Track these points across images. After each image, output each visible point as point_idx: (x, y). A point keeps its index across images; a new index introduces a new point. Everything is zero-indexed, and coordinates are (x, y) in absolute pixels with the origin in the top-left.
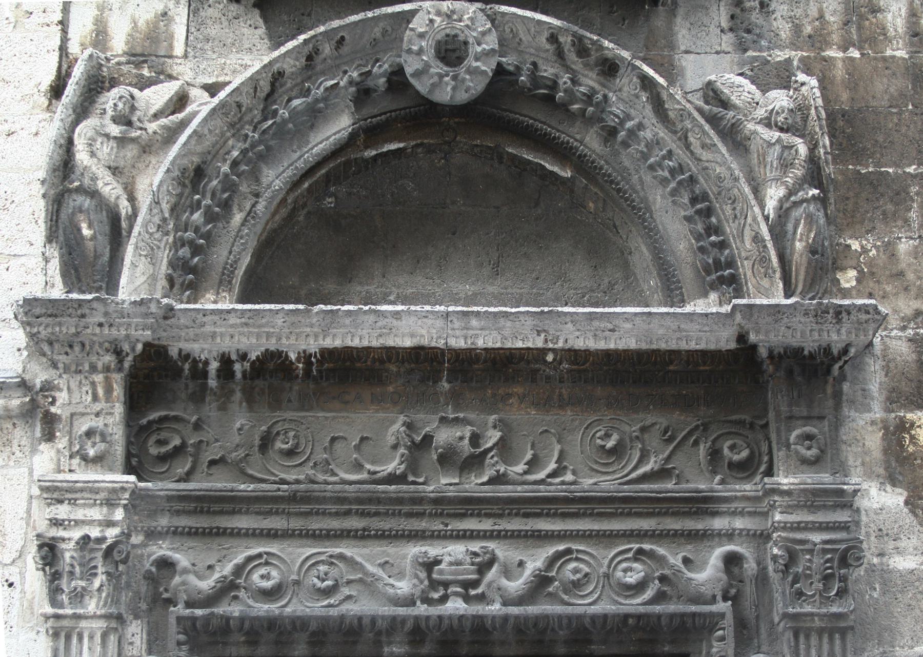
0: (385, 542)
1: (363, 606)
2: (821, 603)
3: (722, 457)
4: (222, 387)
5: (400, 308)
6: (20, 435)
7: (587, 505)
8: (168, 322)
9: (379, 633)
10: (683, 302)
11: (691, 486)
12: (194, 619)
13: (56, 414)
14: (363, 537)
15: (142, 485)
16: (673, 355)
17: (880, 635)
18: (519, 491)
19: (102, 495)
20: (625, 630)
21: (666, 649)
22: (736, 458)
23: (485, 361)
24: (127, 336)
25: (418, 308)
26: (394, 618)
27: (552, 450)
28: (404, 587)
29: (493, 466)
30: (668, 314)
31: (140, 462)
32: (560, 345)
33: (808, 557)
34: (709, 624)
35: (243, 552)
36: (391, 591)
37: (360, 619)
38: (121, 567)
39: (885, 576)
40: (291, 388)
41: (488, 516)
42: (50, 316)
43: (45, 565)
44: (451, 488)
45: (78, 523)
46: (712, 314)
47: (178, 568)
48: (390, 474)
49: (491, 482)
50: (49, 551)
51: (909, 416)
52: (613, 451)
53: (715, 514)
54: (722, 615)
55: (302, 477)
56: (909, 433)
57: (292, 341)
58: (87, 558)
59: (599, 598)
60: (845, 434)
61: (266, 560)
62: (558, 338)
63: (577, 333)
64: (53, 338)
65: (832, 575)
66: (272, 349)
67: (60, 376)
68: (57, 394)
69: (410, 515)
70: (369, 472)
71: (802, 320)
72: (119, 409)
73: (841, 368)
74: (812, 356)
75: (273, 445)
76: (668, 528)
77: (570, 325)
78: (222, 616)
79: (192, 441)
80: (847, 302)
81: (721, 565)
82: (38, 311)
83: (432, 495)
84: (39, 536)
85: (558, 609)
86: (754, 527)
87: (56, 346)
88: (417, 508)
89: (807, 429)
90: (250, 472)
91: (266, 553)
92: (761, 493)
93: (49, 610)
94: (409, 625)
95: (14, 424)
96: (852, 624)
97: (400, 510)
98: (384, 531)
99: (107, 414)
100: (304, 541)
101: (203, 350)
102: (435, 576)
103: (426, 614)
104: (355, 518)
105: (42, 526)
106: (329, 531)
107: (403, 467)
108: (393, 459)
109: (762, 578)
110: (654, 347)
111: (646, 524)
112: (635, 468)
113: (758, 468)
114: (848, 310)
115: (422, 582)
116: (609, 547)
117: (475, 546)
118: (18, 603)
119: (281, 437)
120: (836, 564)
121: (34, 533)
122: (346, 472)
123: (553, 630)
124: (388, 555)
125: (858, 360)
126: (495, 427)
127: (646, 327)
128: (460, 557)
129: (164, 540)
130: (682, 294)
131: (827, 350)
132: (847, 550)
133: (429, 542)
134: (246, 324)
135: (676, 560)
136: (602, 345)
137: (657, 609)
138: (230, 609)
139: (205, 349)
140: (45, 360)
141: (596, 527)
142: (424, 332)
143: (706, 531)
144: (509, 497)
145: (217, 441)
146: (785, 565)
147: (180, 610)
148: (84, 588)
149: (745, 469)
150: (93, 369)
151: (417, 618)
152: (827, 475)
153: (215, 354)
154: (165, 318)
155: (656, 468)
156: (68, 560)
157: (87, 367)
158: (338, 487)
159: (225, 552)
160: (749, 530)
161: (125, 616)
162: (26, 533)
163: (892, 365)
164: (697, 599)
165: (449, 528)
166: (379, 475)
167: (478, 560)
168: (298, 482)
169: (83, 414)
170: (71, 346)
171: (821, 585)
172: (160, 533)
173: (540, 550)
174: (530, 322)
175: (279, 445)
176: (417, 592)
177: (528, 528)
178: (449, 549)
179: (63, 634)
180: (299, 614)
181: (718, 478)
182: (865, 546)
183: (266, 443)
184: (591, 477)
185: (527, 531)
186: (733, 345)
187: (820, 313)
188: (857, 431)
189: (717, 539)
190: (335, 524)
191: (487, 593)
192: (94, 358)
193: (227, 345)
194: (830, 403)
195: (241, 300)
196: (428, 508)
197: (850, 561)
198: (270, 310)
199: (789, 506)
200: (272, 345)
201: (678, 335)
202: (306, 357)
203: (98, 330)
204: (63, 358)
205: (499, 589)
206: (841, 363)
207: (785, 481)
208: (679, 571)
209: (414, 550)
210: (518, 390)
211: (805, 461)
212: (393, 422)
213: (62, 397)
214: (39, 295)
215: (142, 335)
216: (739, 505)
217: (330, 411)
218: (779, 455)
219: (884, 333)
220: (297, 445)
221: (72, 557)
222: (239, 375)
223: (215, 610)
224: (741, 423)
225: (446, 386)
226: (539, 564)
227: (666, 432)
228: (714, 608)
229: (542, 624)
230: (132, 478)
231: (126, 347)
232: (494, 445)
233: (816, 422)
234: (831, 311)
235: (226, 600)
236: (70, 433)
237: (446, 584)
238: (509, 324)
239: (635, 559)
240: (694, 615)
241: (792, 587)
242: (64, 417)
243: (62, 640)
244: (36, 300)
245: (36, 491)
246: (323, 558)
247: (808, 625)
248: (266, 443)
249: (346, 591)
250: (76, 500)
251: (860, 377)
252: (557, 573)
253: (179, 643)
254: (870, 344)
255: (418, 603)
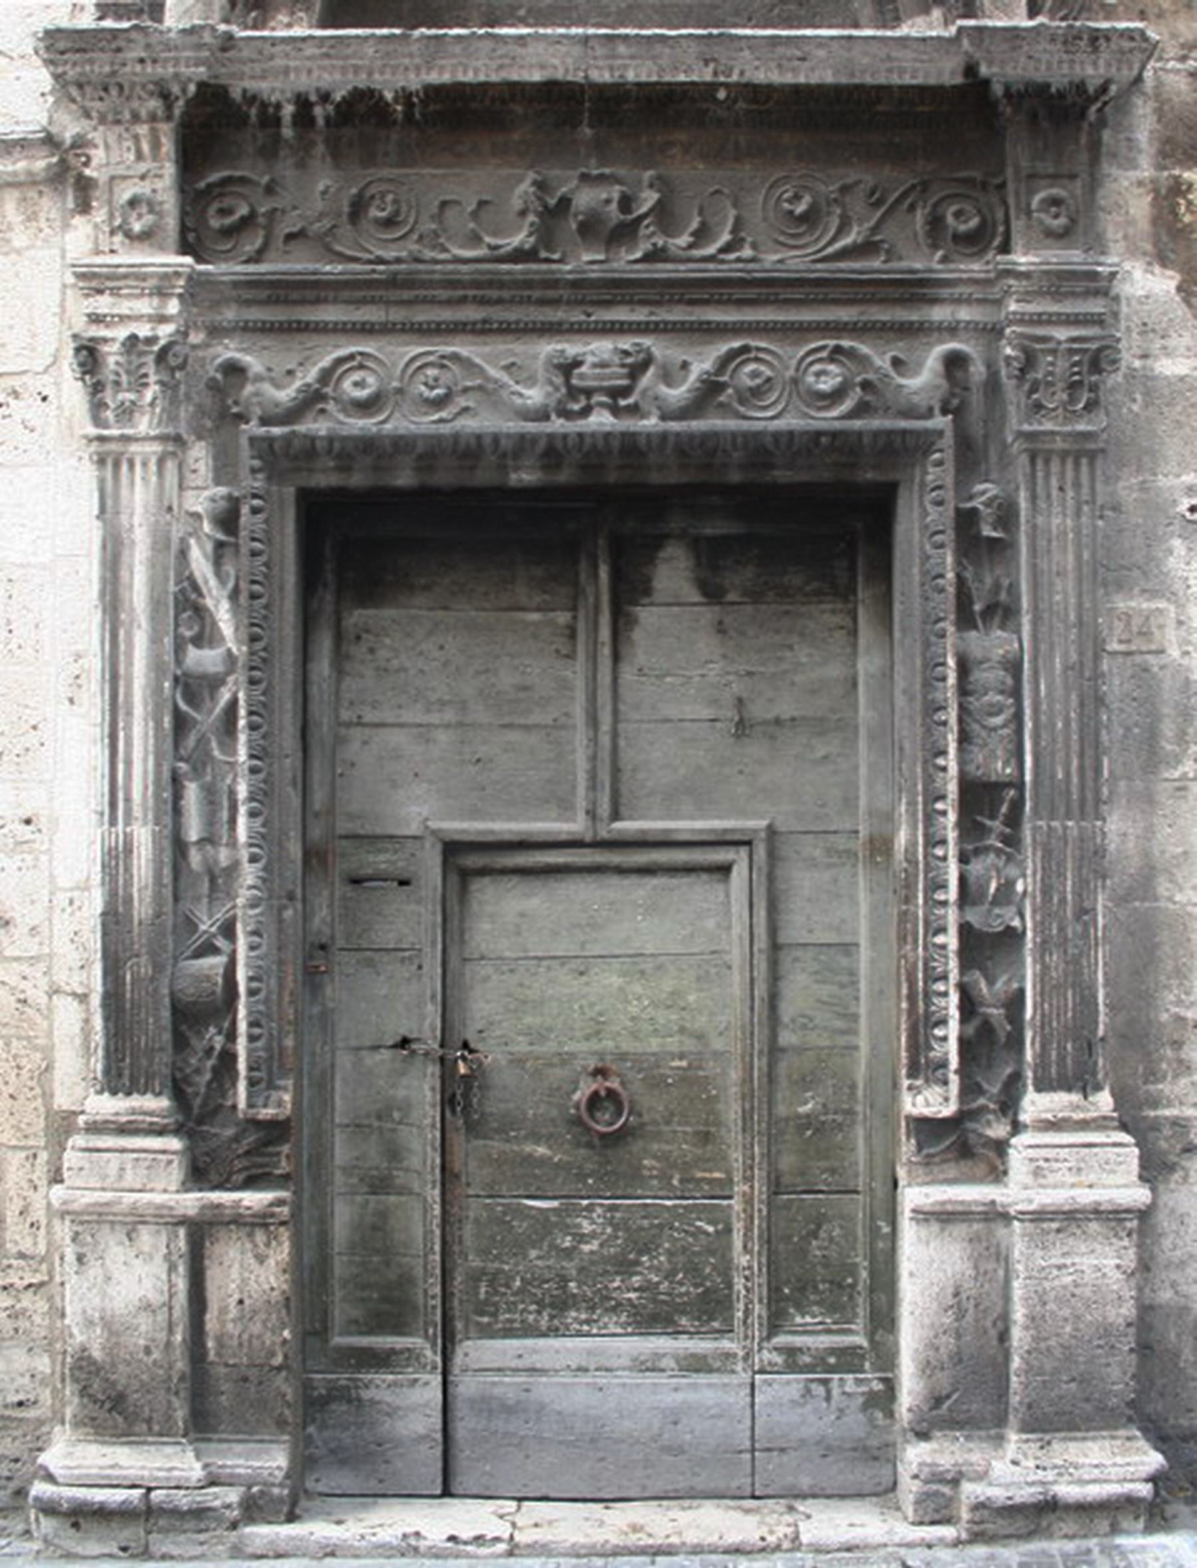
0: (509, 338)
1: (482, 422)
2: (1065, 418)
3: (946, 227)
4: (299, 138)
5: (525, 31)
6: (49, 206)
7: (770, 289)
8: (227, 55)
9: (504, 455)
10: (897, 20)
11: (904, 264)
12: (270, 440)
13: (90, 179)
14: (483, 332)
15: (201, 267)
16: (882, 91)
17: (1140, 460)
18: (681, 271)
19: (152, 282)
20: (817, 451)
21: (869, 476)
22: (962, 228)
23: (637, 99)
24: (176, 75)
25: (549, 31)
26: (522, 437)
27: (726, 216)
28: (534, 396)
29: (649, 238)
30: (873, 38)
31: (198, 239)
32: (735, 78)
33: (1050, 359)
34: (922, 444)
35: (330, 353)
36: (519, 401)
37: (479, 437)
38: (178, 375)
39: (1147, 383)
40: (388, 138)
41: (643, 303)
42: (78, 51)
43: (84, 373)
44: (595, 267)
45: (123, 318)
46: (932, 38)
47: (250, 374)
48: (516, 250)
49: (648, 258)
50: (89, 356)
51: (1186, 175)
52: (804, 218)
53: (935, 301)
54: (940, 433)
55: (404, 254)
56: (1185, 198)
57: (387, 76)
58: (136, 363)
59: (784, 410)
60: (1105, 197)
61: (359, 362)
62: (731, 70)
63: (757, 63)
64: (83, 79)
65: (1080, 383)
66: (361, 86)
67: (95, 129)
68: (92, 152)
69: (542, 302)
70: (490, 247)
71: (1048, 47)
72: (169, 170)
73: (1100, 110)
74: (1061, 95)
75: (366, 212)
76: (873, 318)
77: (747, 53)
78: (305, 436)
79: (263, 210)
80: (1105, 25)
81: (940, 368)
82: (61, 45)
83: (570, 277)
84: (75, 337)
85: (732, 424)
86: (985, 319)
87: (88, 89)
88: (551, 294)
89: (1055, 191)
90: (338, 248)
91: (361, 354)
92: (992, 275)
93: (93, 431)
94: (542, 445)
95: (40, 192)
96: (1101, 445)
97: (529, 297)
98: (509, 324)
99: (156, 176)
100: (406, 337)
101: (273, 90)
102: (574, 381)
103: (562, 430)
104: (474, 307)
105: (79, 323)
106: (439, 324)
107: (532, 239)
108: (520, 229)
109: (993, 386)
110: (857, 81)
111: (845, 314)
112: (830, 243)
113: (990, 242)
114: (1107, 35)
115: (557, 389)
116: (798, 343)
117: (626, 343)
118: (54, 421)
119: (377, 202)
120: (1085, 369)
121: (69, 333)
122: (461, 247)
123: (724, 451)
124: (515, 355)
125: (1121, 101)
126: (651, 186)
127: (846, 55)
128: (606, 356)
129: (232, 339)
130: (896, 10)
131: (1080, 87)
132: (1100, 350)
133: (567, 337)
134: (327, 56)
135: (883, 362)
136: (789, 79)
137: (857, 424)
138: (317, 426)
139: (276, 87)
140: (74, 107)
141: (781, 318)
142: (556, 62)
143: (922, 323)
144: (668, 279)
145: (295, 208)
146: (1021, 370)
147: (253, 428)
148: (133, 403)
149: (975, 242)
150: (136, 118)
151: (551, 436)
152: (1077, 252)
153: (289, 95)
154: (224, 49)
155: (860, 240)
156: (112, 366)
157: (127, 116)
158: (450, 267)
159: (308, 353)
160: (977, 323)
161: (185, 436)
162: (60, 333)
163: (1166, 108)
164: (909, 412)
165: (593, 318)
166: (502, 251)
167: (630, 360)
168: (398, 260)
169: (125, 178)
170: (106, 89)
171: (1065, 397)
172: (225, 329)
173: (712, 347)
174: (694, 48)
175: (374, 213)
176: (552, 402)
177: (693, 318)
178: (592, 347)
179: (110, 462)
180: (402, 432)
181: (940, 253)
182: (1122, 345)
183: (358, 209)
184: (776, 252)
185: (692, 323)
186: (959, 80)
187: (1071, 39)
188: (1120, 193)
189: (936, 335)
190: (446, 315)
191: (642, 404)
192: (135, 104)
193: (305, 83)
194: (1084, 157)
195: (323, 25)
196: (565, 293)
197: (1104, 365)
198: (357, 37)
199: (1028, 293)
200: (362, 81)
201: (888, 65)
202: (406, 97)
203: (138, 68)
204: (97, 104)
205: (656, 398)
206: (1099, 104)
207: (1023, 260)
208: (886, 376)
209: (548, 348)
210: (683, 136)
211: (1050, 234)
212: (521, 180)
213: (98, 155)
214: (65, 24)
215: (194, 72)
216: (965, 290)
217: (437, 166)
218: (1017, 225)
219: (1159, 65)
220: (397, 213)
221: (117, 363)
222: (320, 122)
223: (296, 428)
224: (969, 182)
225: (588, 131)
226: (707, 365)
227: (872, 193)
228: (929, 424)
229: (709, 444)
230: (188, 260)
231: (176, 89)
232: (651, 210)
233: (1066, 181)
234: (1085, 37)
235: (310, 415)
236: (110, 202)
237: (589, 392)
238: (667, 50)
239: (831, 360)
240: (904, 432)
241: (1029, 397)
242: (101, 182)
243: (109, 467)
244: (59, 30)
245: (71, 280)
246: (431, 358)
247: (1047, 446)
248: (358, 209)
249: (462, 402)
250: (120, 288)
251: (1125, 123)
252: (731, 377)
253: (254, 471)
254: (1139, 79)
255: (553, 417)
